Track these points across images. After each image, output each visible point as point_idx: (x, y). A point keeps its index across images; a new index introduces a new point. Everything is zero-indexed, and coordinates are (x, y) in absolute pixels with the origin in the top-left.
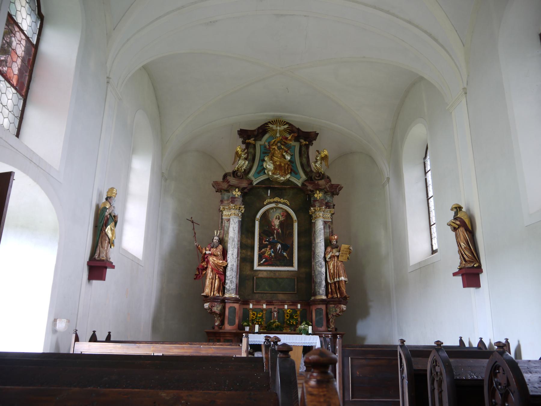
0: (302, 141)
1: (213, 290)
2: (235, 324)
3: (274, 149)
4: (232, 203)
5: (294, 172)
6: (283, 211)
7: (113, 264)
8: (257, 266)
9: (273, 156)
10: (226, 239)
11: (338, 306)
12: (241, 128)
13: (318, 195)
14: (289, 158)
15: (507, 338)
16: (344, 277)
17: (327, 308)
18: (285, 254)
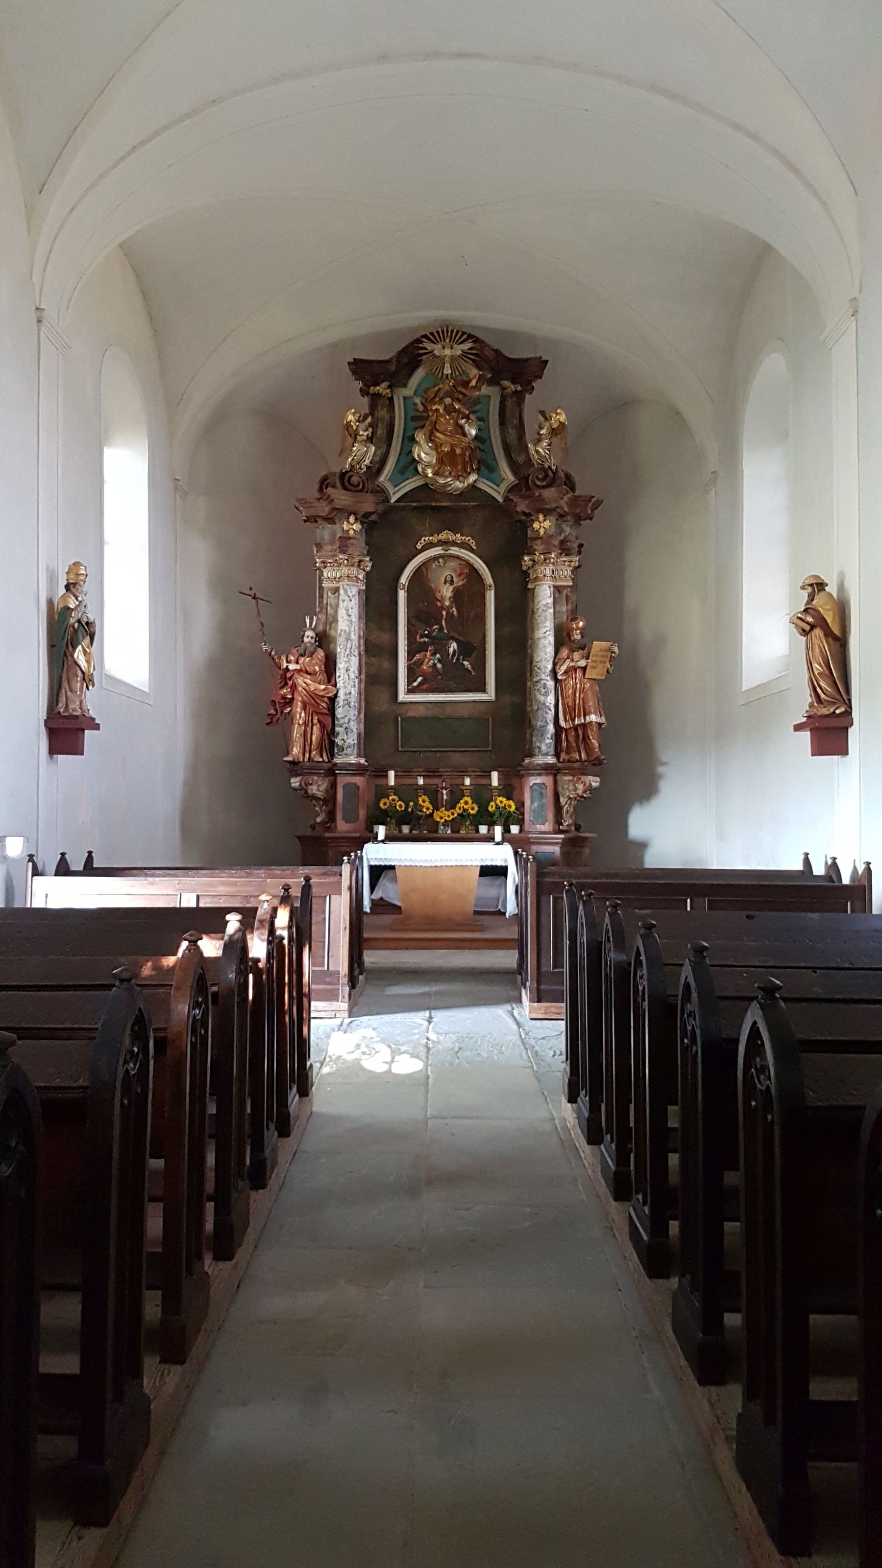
0: (506, 383)
1: (307, 748)
2: (358, 819)
3: (437, 410)
4: (343, 552)
5: (487, 467)
6: (460, 564)
7: (97, 722)
8: (406, 692)
9: (434, 431)
10: (332, 633)
11: (580, 778)
12: (356, 357)
13: (542, 525)
14: (473, 432)
15: (869, 861)
16: (595, 714)
17: (555, 782)
18: (466, 663)
